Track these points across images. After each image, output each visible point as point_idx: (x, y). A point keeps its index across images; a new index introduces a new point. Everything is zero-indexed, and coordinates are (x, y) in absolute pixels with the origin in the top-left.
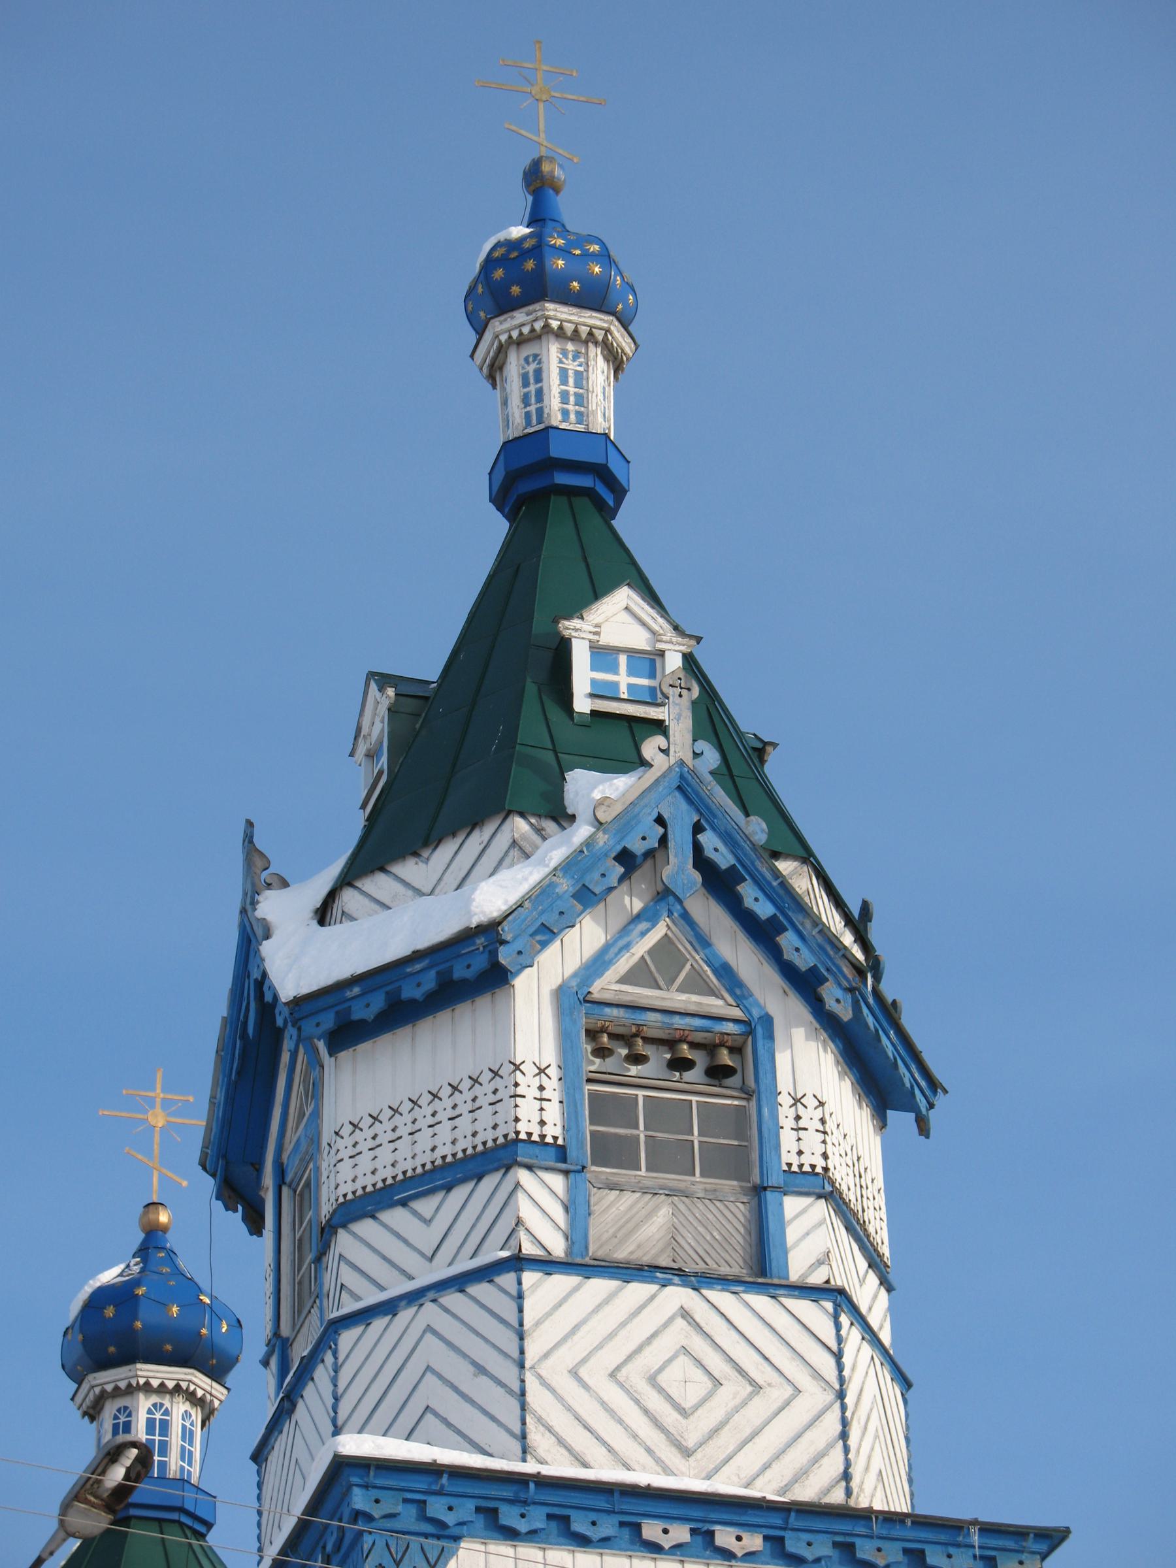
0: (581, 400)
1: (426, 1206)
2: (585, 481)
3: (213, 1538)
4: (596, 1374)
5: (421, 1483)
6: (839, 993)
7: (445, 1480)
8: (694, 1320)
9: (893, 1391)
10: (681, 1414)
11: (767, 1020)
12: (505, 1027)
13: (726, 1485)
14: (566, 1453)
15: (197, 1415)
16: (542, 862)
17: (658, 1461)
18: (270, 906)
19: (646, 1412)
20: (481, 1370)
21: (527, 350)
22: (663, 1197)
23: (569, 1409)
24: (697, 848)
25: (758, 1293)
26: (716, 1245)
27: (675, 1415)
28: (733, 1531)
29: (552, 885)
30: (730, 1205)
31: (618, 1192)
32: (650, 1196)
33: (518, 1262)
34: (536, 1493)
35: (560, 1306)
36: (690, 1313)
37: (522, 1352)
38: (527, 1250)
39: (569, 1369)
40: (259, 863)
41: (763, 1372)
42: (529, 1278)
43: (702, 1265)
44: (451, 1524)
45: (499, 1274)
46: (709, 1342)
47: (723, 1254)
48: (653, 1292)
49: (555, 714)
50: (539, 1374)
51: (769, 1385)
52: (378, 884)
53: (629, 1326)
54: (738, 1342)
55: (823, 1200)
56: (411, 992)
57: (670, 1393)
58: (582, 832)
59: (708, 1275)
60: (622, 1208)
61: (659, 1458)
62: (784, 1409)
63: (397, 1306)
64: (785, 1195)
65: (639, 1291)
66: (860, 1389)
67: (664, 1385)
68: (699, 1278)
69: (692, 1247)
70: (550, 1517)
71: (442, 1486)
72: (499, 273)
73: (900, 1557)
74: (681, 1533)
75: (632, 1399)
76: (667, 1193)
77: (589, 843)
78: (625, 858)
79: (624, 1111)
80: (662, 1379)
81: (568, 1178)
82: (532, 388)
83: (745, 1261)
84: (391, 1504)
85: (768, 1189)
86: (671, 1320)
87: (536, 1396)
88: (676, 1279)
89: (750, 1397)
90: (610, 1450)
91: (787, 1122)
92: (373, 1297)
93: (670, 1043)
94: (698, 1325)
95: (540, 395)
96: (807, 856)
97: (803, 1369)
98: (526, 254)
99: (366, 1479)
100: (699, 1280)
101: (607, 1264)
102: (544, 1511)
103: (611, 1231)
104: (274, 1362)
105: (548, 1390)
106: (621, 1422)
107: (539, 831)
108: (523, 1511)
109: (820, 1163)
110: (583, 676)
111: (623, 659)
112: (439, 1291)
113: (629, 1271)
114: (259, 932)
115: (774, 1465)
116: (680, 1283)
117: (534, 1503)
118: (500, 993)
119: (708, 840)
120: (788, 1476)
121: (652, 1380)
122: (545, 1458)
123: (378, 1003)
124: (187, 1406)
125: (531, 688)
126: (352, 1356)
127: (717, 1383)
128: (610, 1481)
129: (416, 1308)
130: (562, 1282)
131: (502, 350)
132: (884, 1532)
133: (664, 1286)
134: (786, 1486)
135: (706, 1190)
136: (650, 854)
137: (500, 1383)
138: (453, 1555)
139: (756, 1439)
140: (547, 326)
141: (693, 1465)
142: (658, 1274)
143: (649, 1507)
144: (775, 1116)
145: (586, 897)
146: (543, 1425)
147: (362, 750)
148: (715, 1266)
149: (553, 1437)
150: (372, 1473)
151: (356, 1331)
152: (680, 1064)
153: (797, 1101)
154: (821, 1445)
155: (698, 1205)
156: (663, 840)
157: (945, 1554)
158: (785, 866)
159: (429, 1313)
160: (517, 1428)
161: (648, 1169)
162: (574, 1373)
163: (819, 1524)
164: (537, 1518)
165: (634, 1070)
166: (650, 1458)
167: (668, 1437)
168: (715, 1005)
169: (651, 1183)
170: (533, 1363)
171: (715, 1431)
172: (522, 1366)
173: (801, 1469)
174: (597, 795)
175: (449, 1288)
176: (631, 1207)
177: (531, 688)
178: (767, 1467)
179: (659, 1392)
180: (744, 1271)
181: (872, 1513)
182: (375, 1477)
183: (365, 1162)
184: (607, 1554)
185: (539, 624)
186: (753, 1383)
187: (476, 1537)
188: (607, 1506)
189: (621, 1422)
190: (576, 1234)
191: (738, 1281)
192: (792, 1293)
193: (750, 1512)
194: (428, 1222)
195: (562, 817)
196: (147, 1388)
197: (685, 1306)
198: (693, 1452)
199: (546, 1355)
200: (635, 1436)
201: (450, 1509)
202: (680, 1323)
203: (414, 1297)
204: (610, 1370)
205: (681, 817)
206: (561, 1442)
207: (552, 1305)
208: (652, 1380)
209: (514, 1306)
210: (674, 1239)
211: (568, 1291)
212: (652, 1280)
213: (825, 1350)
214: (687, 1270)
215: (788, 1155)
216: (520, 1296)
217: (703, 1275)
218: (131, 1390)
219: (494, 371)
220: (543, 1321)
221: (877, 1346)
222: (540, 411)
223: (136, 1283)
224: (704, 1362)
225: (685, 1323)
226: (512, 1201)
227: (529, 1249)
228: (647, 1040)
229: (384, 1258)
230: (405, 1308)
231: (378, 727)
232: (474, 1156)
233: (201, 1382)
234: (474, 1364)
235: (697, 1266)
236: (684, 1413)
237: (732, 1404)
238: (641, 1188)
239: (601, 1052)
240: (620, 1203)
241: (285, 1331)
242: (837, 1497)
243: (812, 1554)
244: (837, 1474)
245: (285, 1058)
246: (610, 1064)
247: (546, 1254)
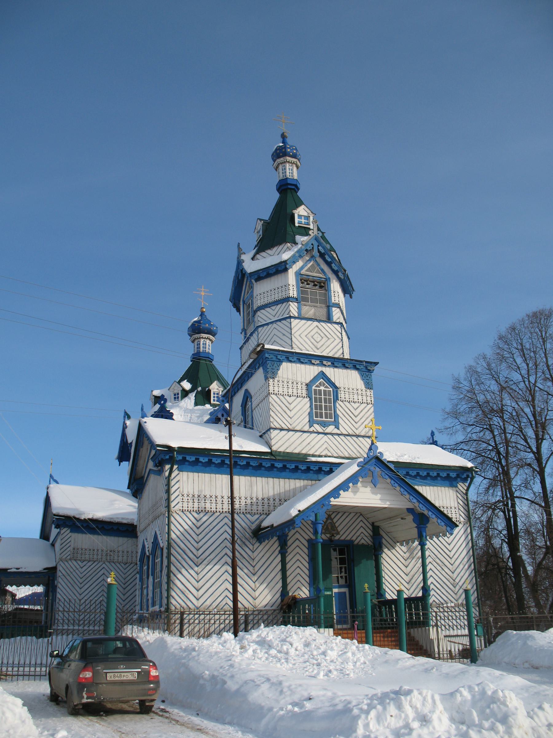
0: (292, 173)
1: (273, 308)
2: (293, 187)
3: (213, 362)
5: (277, 353)
6: (341, 274)
9: (347, 340)
11: (329, 278)
12: (287, 278)
13: (324, 354)
15: (210, 342)
16: (293, 251)
17: (313, 350)
18: (243, 257)
19: (311, 342)
20: (284, 335)
21: (283, 165)
24: (318, 249)
29: (295, 255)
33: (290, 317)
40: (240, 250)
42: (292, 320)
49: (292, 226)
52: (263, 254)
56: (271, 272)
58: (300, 246)
65: (310, 322)
72: (278, 151)
74: (318, 362)
77: (301, 248)
78: (307, 250)
79: (306, 293)
82: (284, 171)
84: (272, 356)
86: (315, 327)
87: (294, 339)
91: (333, 295)
93: (313, 282)
95: (285, 172)
96: (335, 252)
98: (283, 148)
100: (319, 321)
104: (243, 333)
107: (292, 245)
109: (338, 302)
110: (297, 220)
111: (303, 217)
114: (242, 261)
118: (286, 272)
119: (320, 248)
123: (265, 274)
124: (209, 341)
125: (288, 222)
127: (322, 338)
130: (297, 321)
131: (279, 164)
136: (310, 250)
137: (287, 337)
140: (287, 161)
144: (331, 294)
145: (301, 257)
147: (256, 231)
151: (262, 328)
152: (315, 285)
153: (334, 292)
154: (339, 348)
156: (313, 248)
158: (332, 253)
159: (275, 325)
162: (300, 335)
163: (340, 361)
165: (307, 286)
168: (321, 275)
171: (322, 346)
172: (291, 334)
174: (302, 240)
177: (288, 222)
178: (330, 351)
183: (262, 300)
185: (288, 211)
190: (299, 312)
191: (326, 321)
194: (274, 310)
195: (296, 243)
196: (203, 338)
199: (295, 333)
202: (316, 328)
203: (272, 323)
205: (316, 244)
208: (312, 337)
209: (290, 324)
215: (333, 301)
216: (291, 323)
218: (200, 338)
219: (277, 169)
222: (285, 175)
223: (201, 320)
227: (292, 315)
228: (310, 281)
231: (259, 227)
233: (211, 337)
236: (317, 343)
239: (302, 283)
241: (245, 328)
242: (342, 356)
245: (245, 283)
246: (303, 285)
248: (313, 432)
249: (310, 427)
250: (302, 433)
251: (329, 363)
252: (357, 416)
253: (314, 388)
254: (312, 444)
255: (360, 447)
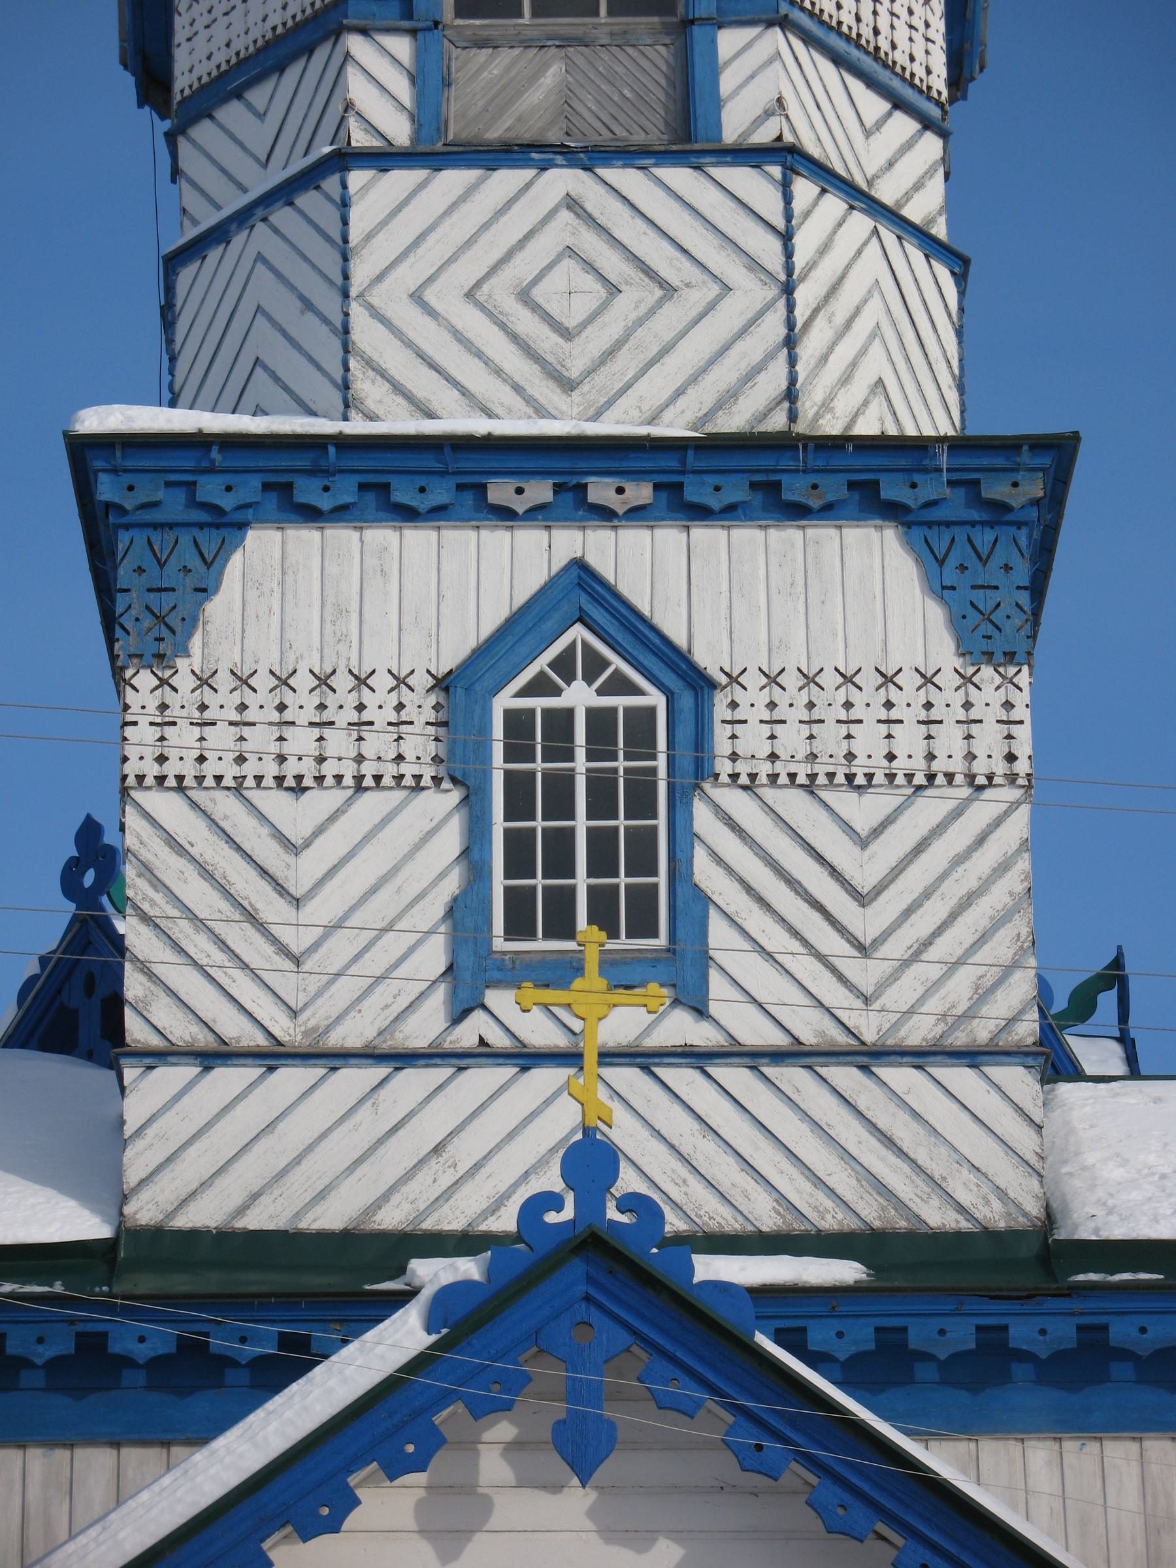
1: (258, 96)
4: (441, 296)
5: (186, 460)
7: (215, 454)
8: (585, 211)
10: (562, 336)
14: (404, 402)
17: (530, 400)
19: (514, 338)
20: (308, 305)
22: (553, 50)
23: (409, 344)
25: (674, 165)
26: (627, 107)
27: (555, 338)
28: (613, 482)
30: (648, 51)
31: (490, 50)
32: (535, 50)
34: (338, 458)
35: (400, 211)
36: (578, 201)
37: (346, 277)
38: (357, 141)
39: (410, 293)
41: (679, 269)
42: (357, 178)
43: (606, 134)
44: (228, 508)
45: (324, 178)
46: (605, 237)
47: (636, 118)
48: (528, 180)
50: (369, 303)
51: (688, 285)
53: (493, 229)
54: (645, 233)
55: (777, 30)
57: (549, 310)
59: (602, 149)
60: (495, 72)
61: (531, 397)
62: (707, 314)
63: (228, 231)
64: (720, 28)
65: (508, 179)
66: (834, 279)
67: (540, 301)
68: (590, 154)
69: (592, 112)
70: (852, 485)
71: (213, 461)
73: (844, 493)
74: (540, 491)
75: (495, 323)
76: (557, 43)
80: (537, 293)
81: (416, 40)
83: (667, 124)
85: (696, 23)
87: (365, 333)
88: (559, 159)
89: (660, 303)
90: (464, 392)
92: (210, 219)
94: (590, 216)
97: (736, 259)
99: (113, 463)
101: (461, 149)
102: (353, 481)
103: (480, 104)
105: (382, 323)
106: (479, 354)
108: (326, 483)
112: (267, 206)
113: (492, 156)
115: (690, 391)
116: (564, 163)
117: (341, 471)
120: (709, 401)
121: (525, 296)
122: (376, 411)
126: (926, 298)
127: (614, 290)
128: (436, 433)
129: (247, 231)
130: (402, 179)
132: (820, 463)
133: (544, 169)
134: (705, 415)
135: (612, 34)
138: (237, 547)
139: (667, 359)
141: (576, 401)
142: (534, 155)
143: (494, 463)
146: (373, 369)
148: (625, 134)
149: (387, 385)
150: (118, 454)
154: (757, 357)
155: (603, 56)
157: (908, 484)
159: (260, 238)
160: (338, 374)
161: (535, 14)
162: (417, 297)
164: (736, 491)
166: (519, 398)
167: (543, 368)
169: (535, 33)
170: (361, 289)
171: (610, 354)
172: (346, 295)
173: (728, 392)
175: (274, 202)
176: (508, 69)
178: (679, 393)
179: (533, 310)
180: (665, 137)
181: (799, 440)
182: (123, 457)
184: (446, 527)
186: (665, 285)
187: (267, 521)
188: (438, 466)
189: (479, 354)
192: (723, 160)
193: (633, 455)
197: (572, 193)
198: (578, 384)
199: (380, 278)
200: (498, 372)
201: (229, 489)
202: (565, 215)
203: (243, 218)
204: (466, 289)
206: (398, 388)
207: (387, 212)
209: (336, 215)
210: (569, 105)
211: (410, 190)
212: (525, 164)
213: (769, 230)
214: (573, 145)
217: (594, 149)
220: (376, 234)
221: (883, 215)
224: (597, 265)
225: (572, 215)
226: (341, 81)
227: (360, 139)
229: (223, 170)
230: (237, 234)
232: (306, 21)
234: (303, 299)
235: (600, 138)
236: (567, 334)
237: (633, 316)
238: (522, 42)
240: (492, 66)
242: (777, 422)
243: (720, 501)
244: (777, 392)
247: (385, 143)
248: (484, 1053)
249: (458, 1017)
250: (382, 1071)
251: (641, 493)
252: (879, 889)
253: (655, 699)
254: (466, 1151)
255: (888, 1141)
